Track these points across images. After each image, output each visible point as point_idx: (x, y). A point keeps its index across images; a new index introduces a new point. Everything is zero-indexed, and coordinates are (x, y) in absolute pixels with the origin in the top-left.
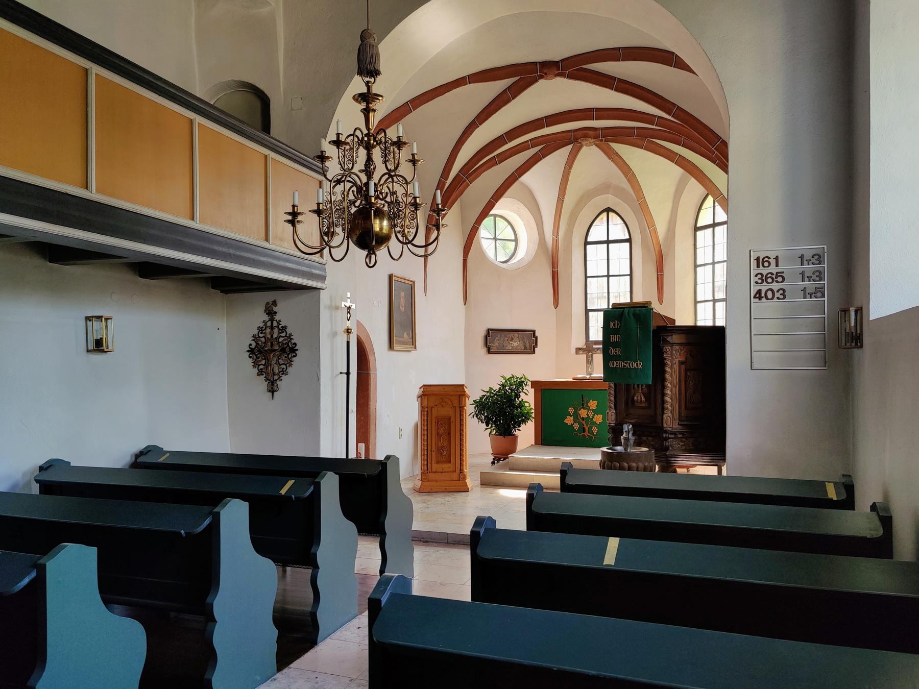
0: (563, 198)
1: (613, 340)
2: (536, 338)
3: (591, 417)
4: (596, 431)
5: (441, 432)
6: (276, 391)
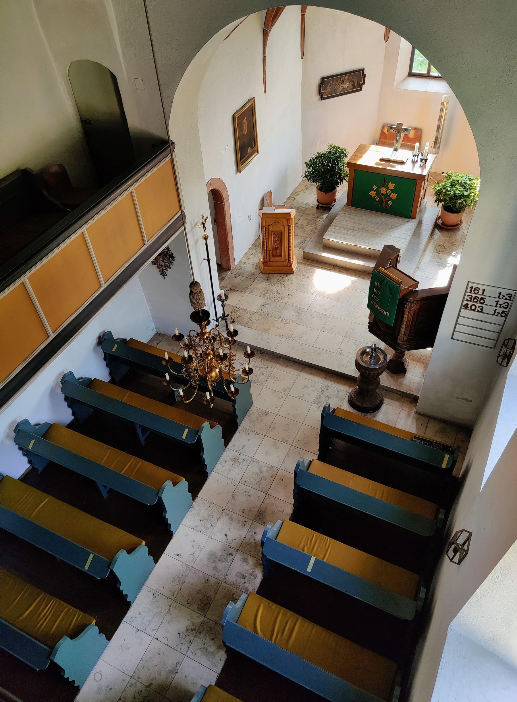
1: (375, 291)
3: (388, 194)
4: (391, 204)
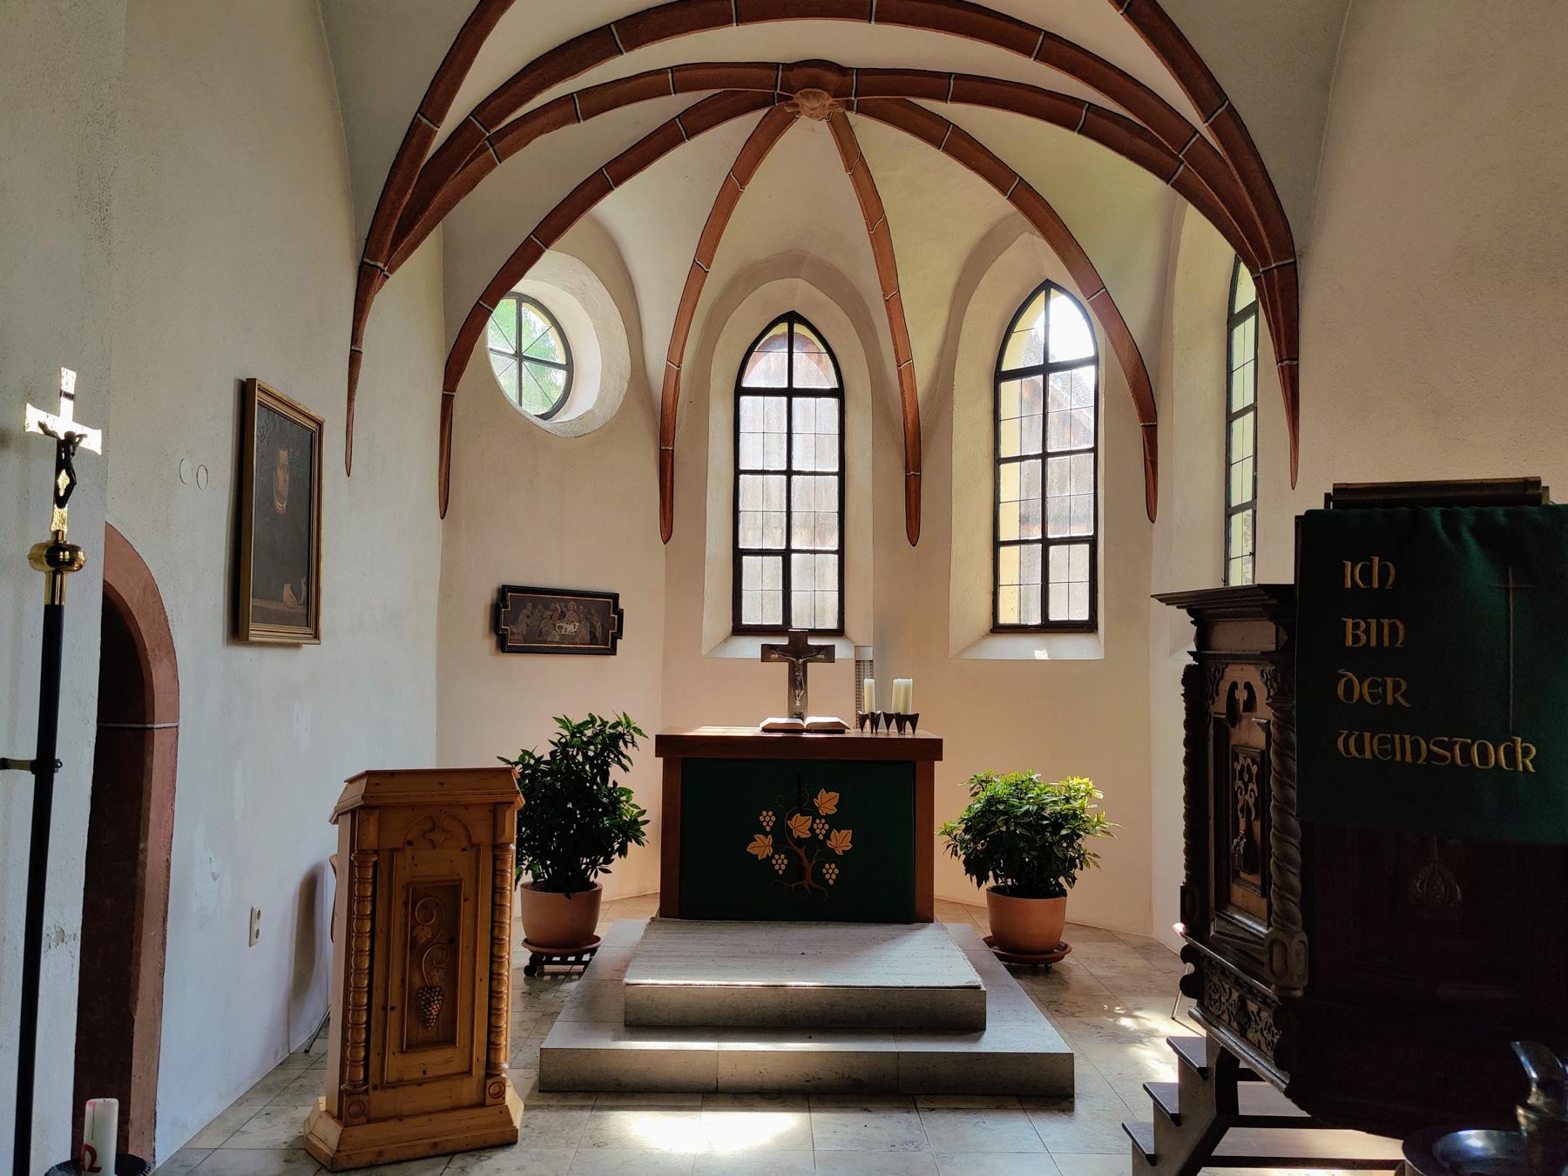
0: (709, 267)
1: (1356, 638)
2: (620, 614)
3: (821, 837)
5: (424, 934)
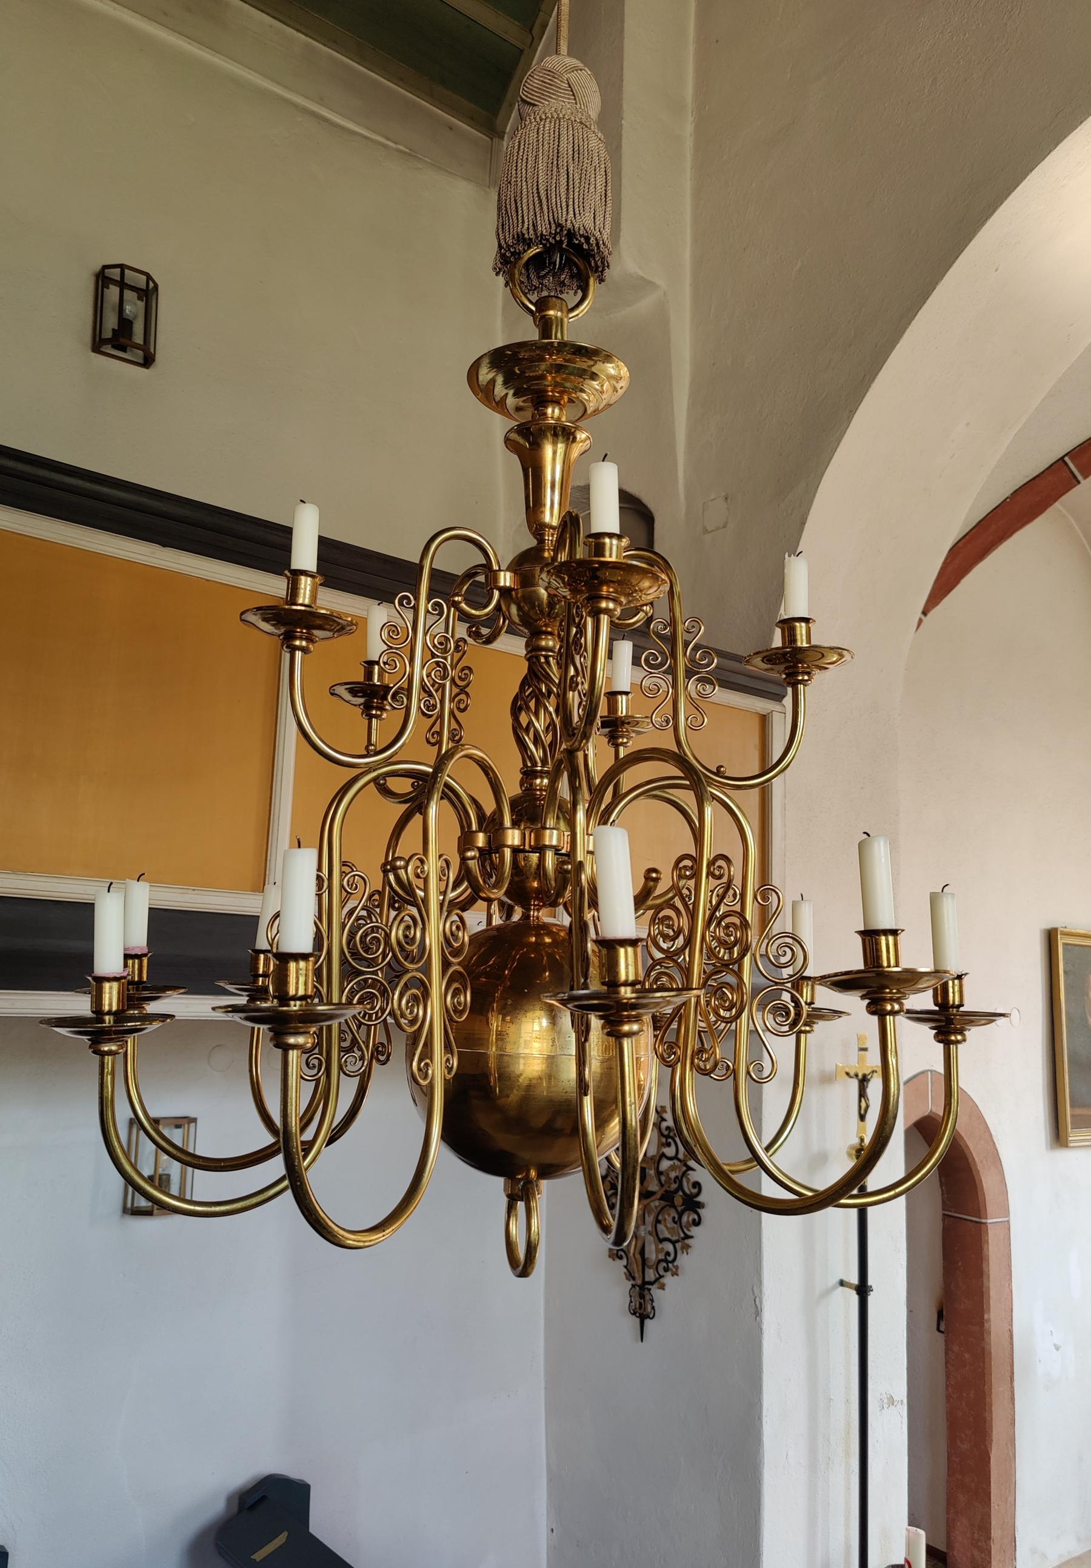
6: (648, 1317)
